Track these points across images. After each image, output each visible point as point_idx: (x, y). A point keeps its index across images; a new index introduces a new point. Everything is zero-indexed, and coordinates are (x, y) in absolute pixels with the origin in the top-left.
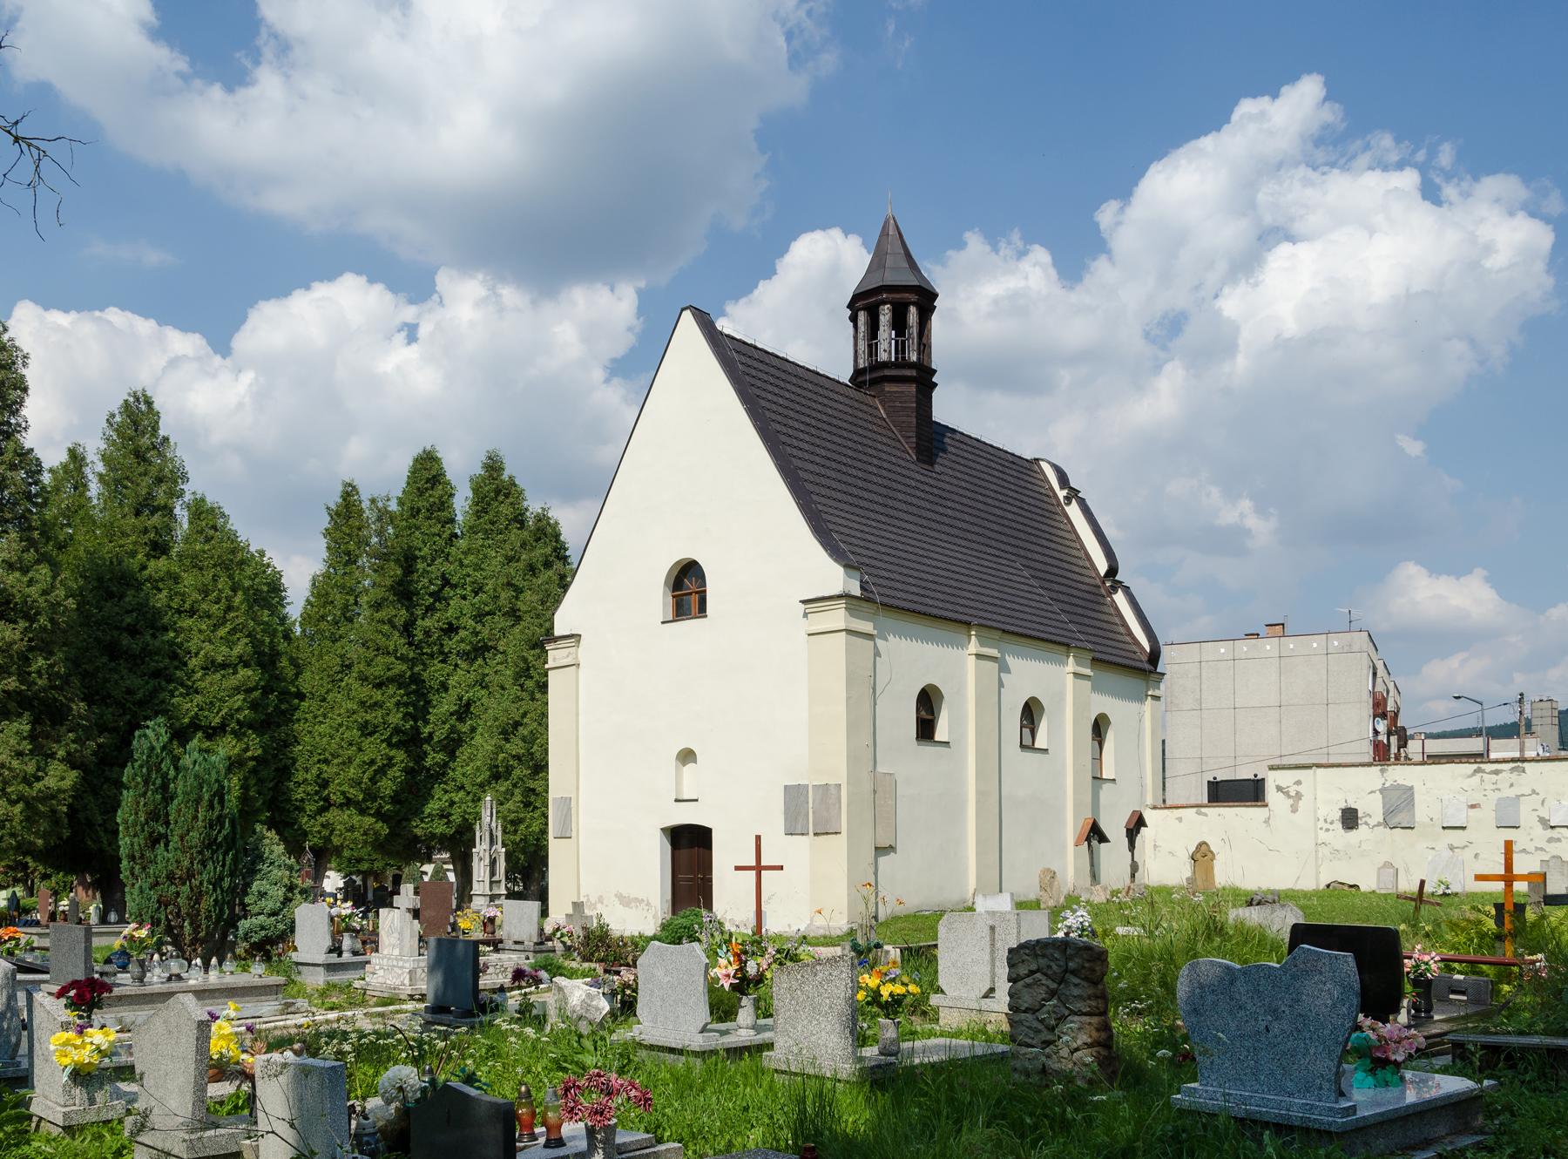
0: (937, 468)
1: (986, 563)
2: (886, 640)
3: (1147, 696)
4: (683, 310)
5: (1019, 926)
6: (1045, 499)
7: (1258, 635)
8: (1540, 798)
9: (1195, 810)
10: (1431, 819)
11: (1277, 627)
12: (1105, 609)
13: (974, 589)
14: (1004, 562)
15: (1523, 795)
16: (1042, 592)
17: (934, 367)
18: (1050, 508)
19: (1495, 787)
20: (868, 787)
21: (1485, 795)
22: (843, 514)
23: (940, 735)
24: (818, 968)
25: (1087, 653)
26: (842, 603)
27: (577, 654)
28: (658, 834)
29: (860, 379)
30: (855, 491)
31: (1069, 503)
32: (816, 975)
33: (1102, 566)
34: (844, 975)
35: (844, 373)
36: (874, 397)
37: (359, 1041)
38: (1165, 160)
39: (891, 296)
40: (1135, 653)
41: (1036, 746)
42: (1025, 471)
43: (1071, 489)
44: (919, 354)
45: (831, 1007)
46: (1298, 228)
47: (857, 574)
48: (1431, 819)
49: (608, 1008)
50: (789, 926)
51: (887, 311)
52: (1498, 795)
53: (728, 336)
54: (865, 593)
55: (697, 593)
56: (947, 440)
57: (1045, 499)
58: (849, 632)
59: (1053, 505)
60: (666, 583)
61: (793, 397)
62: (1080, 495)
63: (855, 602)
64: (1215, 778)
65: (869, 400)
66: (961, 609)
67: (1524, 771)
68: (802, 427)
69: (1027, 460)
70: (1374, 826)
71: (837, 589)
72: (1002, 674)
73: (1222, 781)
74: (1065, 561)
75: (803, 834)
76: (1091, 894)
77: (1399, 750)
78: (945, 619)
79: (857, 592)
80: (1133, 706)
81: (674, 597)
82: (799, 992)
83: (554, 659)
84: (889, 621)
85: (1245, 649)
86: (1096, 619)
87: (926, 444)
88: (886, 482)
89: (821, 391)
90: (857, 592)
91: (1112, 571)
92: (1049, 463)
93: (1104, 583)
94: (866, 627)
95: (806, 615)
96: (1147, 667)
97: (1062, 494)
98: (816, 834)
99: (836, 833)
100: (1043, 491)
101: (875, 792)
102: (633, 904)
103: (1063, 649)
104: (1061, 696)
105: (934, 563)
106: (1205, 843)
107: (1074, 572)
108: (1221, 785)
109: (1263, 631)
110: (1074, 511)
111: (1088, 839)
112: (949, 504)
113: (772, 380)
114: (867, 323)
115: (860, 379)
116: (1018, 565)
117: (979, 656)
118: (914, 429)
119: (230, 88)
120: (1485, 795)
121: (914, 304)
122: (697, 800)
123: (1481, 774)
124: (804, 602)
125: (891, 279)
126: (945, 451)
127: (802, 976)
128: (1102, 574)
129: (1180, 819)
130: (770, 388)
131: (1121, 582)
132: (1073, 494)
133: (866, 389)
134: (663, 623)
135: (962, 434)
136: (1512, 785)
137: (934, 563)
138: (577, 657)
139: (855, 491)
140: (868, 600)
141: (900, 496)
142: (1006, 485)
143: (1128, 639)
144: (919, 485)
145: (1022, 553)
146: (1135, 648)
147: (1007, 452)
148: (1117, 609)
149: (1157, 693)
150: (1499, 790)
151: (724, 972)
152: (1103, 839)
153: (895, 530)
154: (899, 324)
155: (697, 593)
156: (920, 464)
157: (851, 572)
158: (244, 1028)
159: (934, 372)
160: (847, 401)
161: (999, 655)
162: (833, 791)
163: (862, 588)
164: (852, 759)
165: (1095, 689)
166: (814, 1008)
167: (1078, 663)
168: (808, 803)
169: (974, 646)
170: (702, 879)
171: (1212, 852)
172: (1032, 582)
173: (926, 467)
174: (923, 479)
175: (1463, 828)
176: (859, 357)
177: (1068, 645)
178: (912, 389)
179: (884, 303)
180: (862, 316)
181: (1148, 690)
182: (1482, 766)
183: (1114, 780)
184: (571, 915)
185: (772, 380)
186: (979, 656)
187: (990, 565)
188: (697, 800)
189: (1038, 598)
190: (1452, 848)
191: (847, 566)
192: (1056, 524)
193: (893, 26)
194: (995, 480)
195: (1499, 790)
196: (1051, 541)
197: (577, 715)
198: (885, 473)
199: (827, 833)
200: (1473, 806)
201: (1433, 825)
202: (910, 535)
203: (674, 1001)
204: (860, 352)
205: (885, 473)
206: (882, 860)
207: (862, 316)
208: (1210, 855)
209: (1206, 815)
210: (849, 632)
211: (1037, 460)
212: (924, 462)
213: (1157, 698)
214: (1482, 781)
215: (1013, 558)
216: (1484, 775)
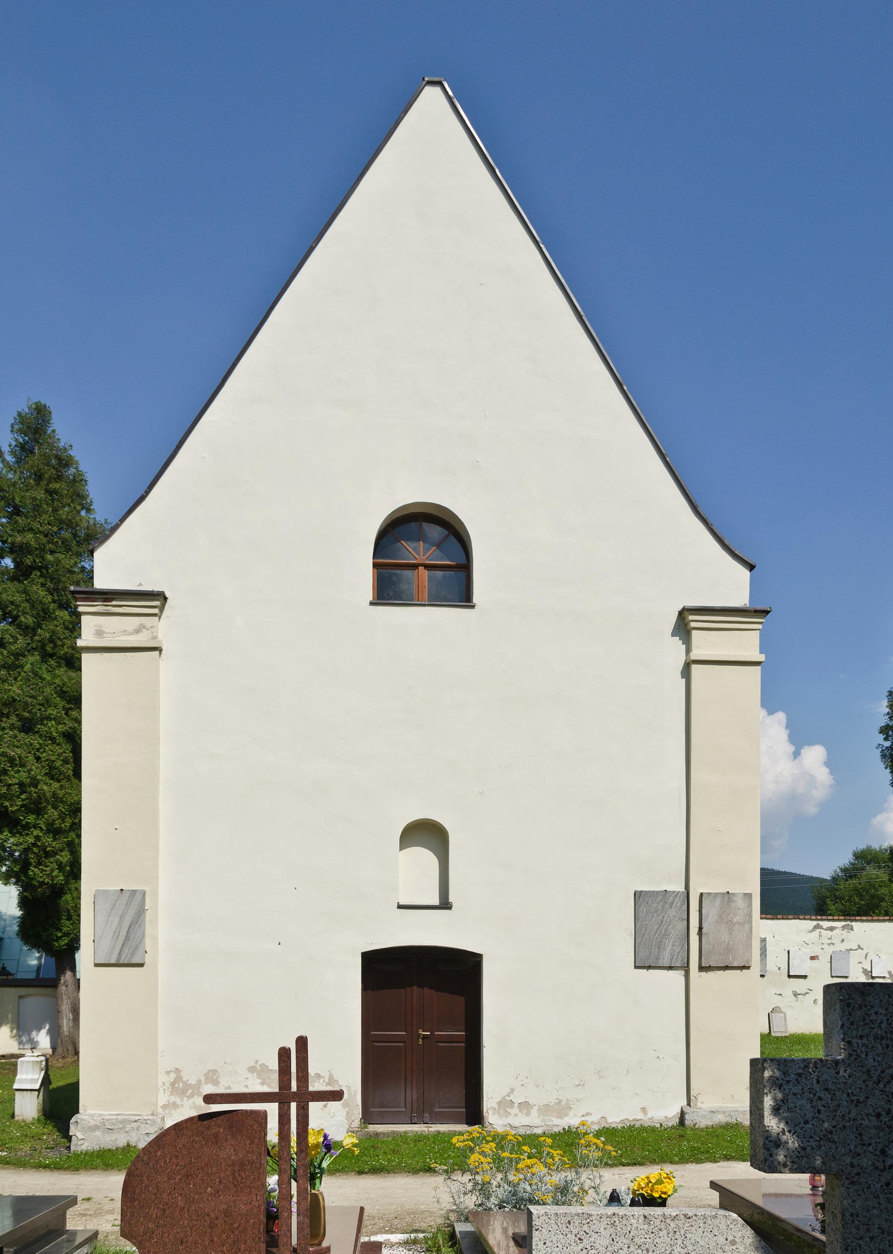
5: (406, 1092)
8: (864, 952)
10: (779, 969)
15: (851, 950)
19: (829, 941)
21: (822, 949)
48: (779, 969)
50: (644, 1110)
52: (831, 949)
55: (428, 567)
67: (852, 929)
83: (99, 633)
120: (822, 949)
123: (819, 930)
136: (843, 941)
138: (155, 638)
150: (833, 944)
162: (740, 903)
175: (805, 977)
182: (820, 922)
190: (796, 994)
195: (833, 944)
199: (726, 968)
200: (812, 958)
201: (780, 974)
206: (22, 1001)
214: (820, 936)
216: (822, 930)
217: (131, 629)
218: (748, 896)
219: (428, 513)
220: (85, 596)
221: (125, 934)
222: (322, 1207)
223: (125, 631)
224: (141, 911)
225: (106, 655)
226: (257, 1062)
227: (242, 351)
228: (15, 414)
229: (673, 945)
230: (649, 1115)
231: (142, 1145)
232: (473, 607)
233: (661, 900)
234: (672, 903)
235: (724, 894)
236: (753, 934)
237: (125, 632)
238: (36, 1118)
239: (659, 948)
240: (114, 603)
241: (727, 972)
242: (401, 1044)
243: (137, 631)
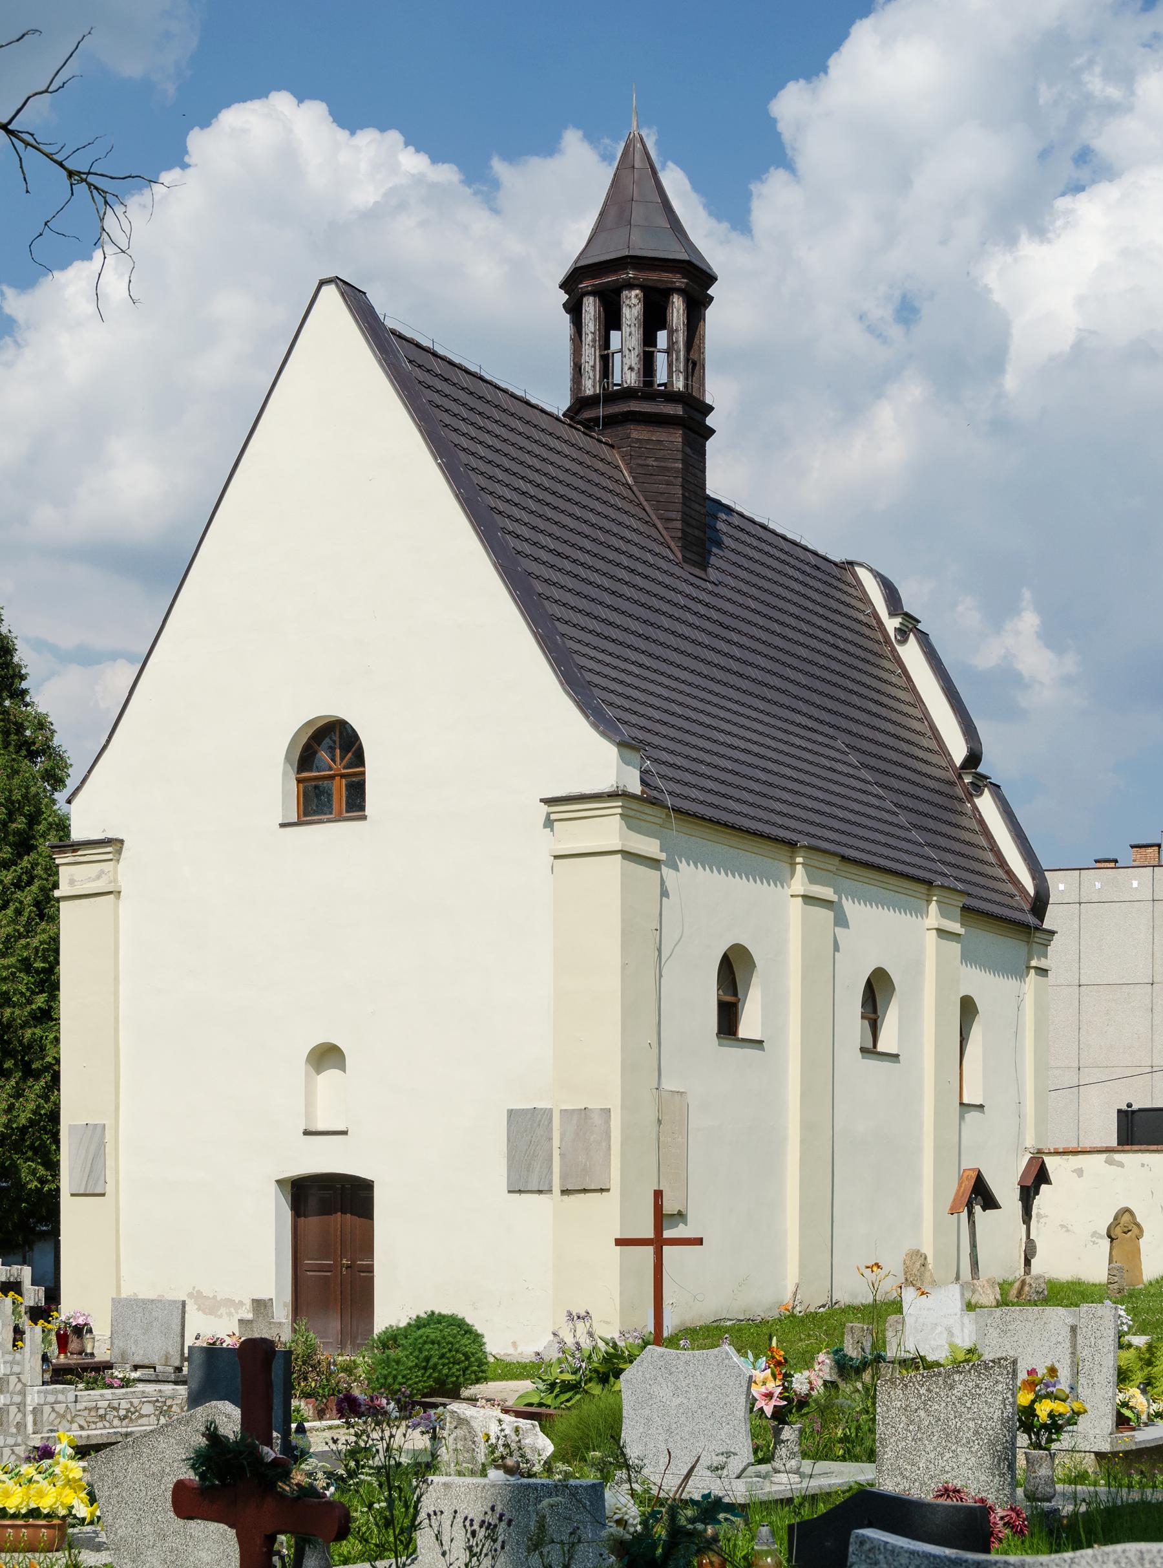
0: (713, 574)
1: (798, 741)
2: (677, 869)
3: (1029, 968)
4: (323, 283)
6: (867, 632)
7: (1116, 861)
9: (1104, 1156)
11: (1150, 850)
12: (965, 822)
13: (790, 785)
14: (820, 738)
16: (881, 792)
17: (708, 400)
18: (875, 647)
20: (651, 1115)
22: (593, 653)
23: (746, 1029)
24: (956, 1377)
25: (956, 897)
26: (616, 807)
27: (116, 872)
28: (273, 1188)
29: (587, 414)
30: (603, 613)
31: (904, 641)
32: (952, 1387)
33: (958, 751)
34: (1000, 1387)
35: (558, 402)
36: (612, 446)
39: (643, 276)
40: (1012, 896)
41: (881, 1048)
42: (835, 583)
43: (907, 615)
44: (686, 379)
45: (976, 1433)
47: (635, 757)
50: (514, 1344)
51: (634, 301)
53: (394, 332)
54: (647, 790)
55: (342, 776)
56: (721, 526)
57: (867, 632)
58: (627, 855)
59: (878, 642)
60: (288, 758)
61: (498, 444)
62: (919, 626)
63: (635, 805)
64: (1130, 1105)
65: (605, 451)
66: (779, 820)
68: (516, 498)
69: (835, 564)
71: (606, 784)
72: (836, 928)
73: (1141, 1110)
74: (903, 740)
75: (540, 1192)
76: (974, 1292)
78: (740, 829)
79: (636, 788)
80: (1010, 984)
81: (299, 781)
82: (922, 1413)
83: (72, 882)
84: (683, 835)
85: (1098, 885)
86: (954, 839)
87: (697, 533)
88: (644, 598)
89: (536, 435)
90: (636, 788)
91: (973, 759)
92: (871, 570)
93: (960, 777)
94: (650, 846)
95: (549, 823)
96: (1031, 919)
97: (892, 624)
98: (565, 1192)
99: (602, 1190)
100: (862, 617)
101: (659, 1122)
102: (223, 1310)
103: (922, 889)
104: (917, 966)
105: (730, 740)
106: (1127, 1210)
107: (917, 758)
108: (1136, 1116)
109: (1127, 856)
110: (911, 654)
111: (970, 1206)
112: (735, 637)
113: (464, 413)
114: (598, 318)
115: (587, 414)
116: (839, 744)
117: (808, 899)
118: (679, 507)
121: (679, 291)
122: (345, 1133)
124: (548, 801)
125: (643, 245)
126: (719, 544)
127: (929, 1390)
128: (958, 766)
129: (1079, 1172)
130: (463, 427)
131: (986, 778)
132: (910, 626)
133: (601, 433)
134: (283, 825)
135: (741, 515)
137: (730, 740)
138: (115, 881)
139: (603, 613)
140: (654, 802)
141: (666, 622)
142: (810, 605)
143: (1000, 873)
144: (691, 604)
145: (844, 723)
146: (1010, 888)
147: (806, 549)
148: (982, 822)
149: (1043, 963)
151: (763, 1390)
152: (990, 1203)
153: (667, 681)
154: (654, 320)
155: (342, 776)
156: (686, 566)
157: (629, 754)
159: (710, 409)
160: (575, 454)
161: (835, 898)
162: (597, 1120)
163: (643, 782)
164: (629, 1068)
165: (968, 957)
166: (948, 1435)
167: (944, 914)
168: (551, 1139)
169: (799, 882)
170: (348, 1267)
171: (1138, 1226)
172: (864, 774)
173: (698, 572)
174: (694, 593)
176: (585, 376)
177: (929, 883)
178: (675, 438)
179: (630, 286)
180: (590, 307)
181: (1030, 959)
183: (982, 1106)
184: (249, 1322)
185: (464, 413)
186: (808, 899)
187: (804, 744)
188: (345, 1133)
189: (876, 802)
191: (622, 745)
192: (884, 675)
194: (795, 598)
196: (881, 704)
197: (116, 980)
198: (638, 581)
199: (585, 1191)
202: (688, 690)
203: (692, 1433)
204: (587, 367)
205: (638, 581)
207: (590, 307)
208: (1135, 1230)
209: (1121, 1165)
210: (627, 855)
211: (851, 563)
212: (695, 564)
213: (1043, 972)
215: (831, 731)
217: (93, 875)
218: (607, 1111)
221: (90, 1166)
223: (90, 878)
224: (102, 1145)
225: (77, 902)
229: (541, 1168)
230: (519, 1351)
232: (364, 818)
233: (530, 1119)
234: (540, 1121)
235: (581, 1110)
236: (612, 1152)
237: (90, 880)
239: (528, 1171)
240: (79, 853)
241: (523, 1195)
242: (329, 1274)
243: (98, 877)
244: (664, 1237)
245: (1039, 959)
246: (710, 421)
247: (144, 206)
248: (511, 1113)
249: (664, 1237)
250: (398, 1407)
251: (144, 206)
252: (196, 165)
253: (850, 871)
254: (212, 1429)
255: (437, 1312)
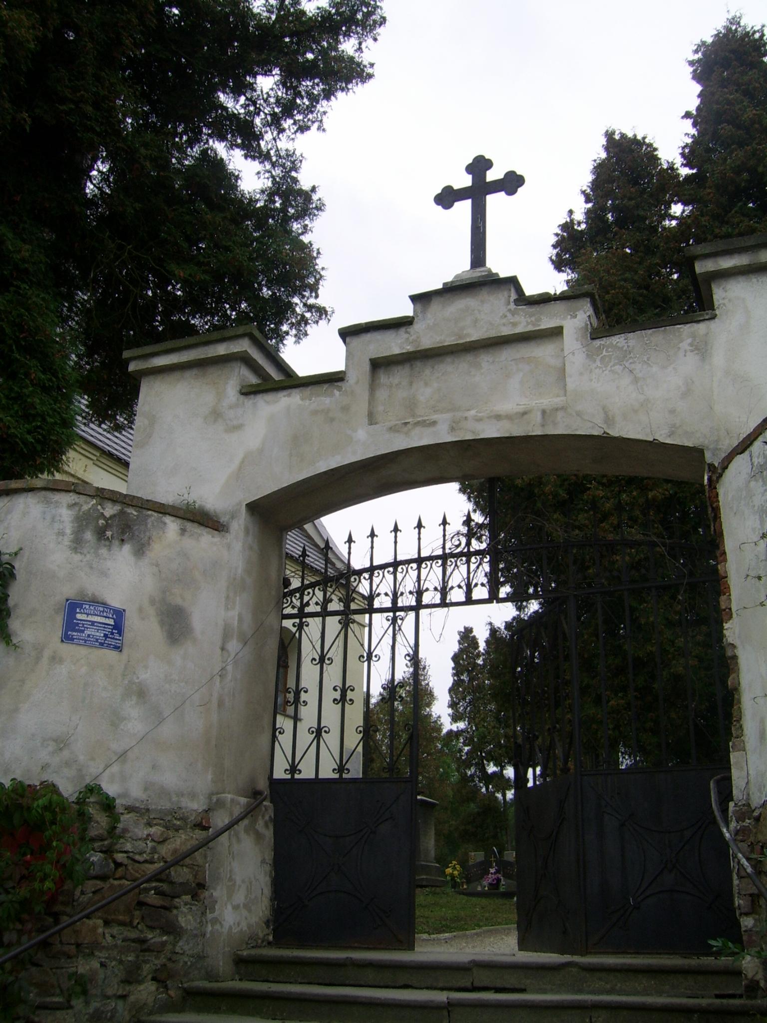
37: (349, 7)
38: (132, 350)
46: (223, 652)
49: (102, 921)
70: (163, 982)
77: (102, 428)
119: (460, 490)
158: (102, 635)
193: (730, 943)
219: (288, 365)
220: (441, 997)
222: (14, 484)
226: (372, 65)
227: (295, 749)
228: (312, 185)
231: (726, 626)
238: (127, 548)
244: (328, 610)
245: (49, 472)
246: (463, 630)
247: (257, 644)
248: (371, 360)
249: (328, 610)
250: (479, 769)
251: (257, 644)
252: (681, 140)
253: (119, 470)
254: (30, 56)
255: (136, 418)
